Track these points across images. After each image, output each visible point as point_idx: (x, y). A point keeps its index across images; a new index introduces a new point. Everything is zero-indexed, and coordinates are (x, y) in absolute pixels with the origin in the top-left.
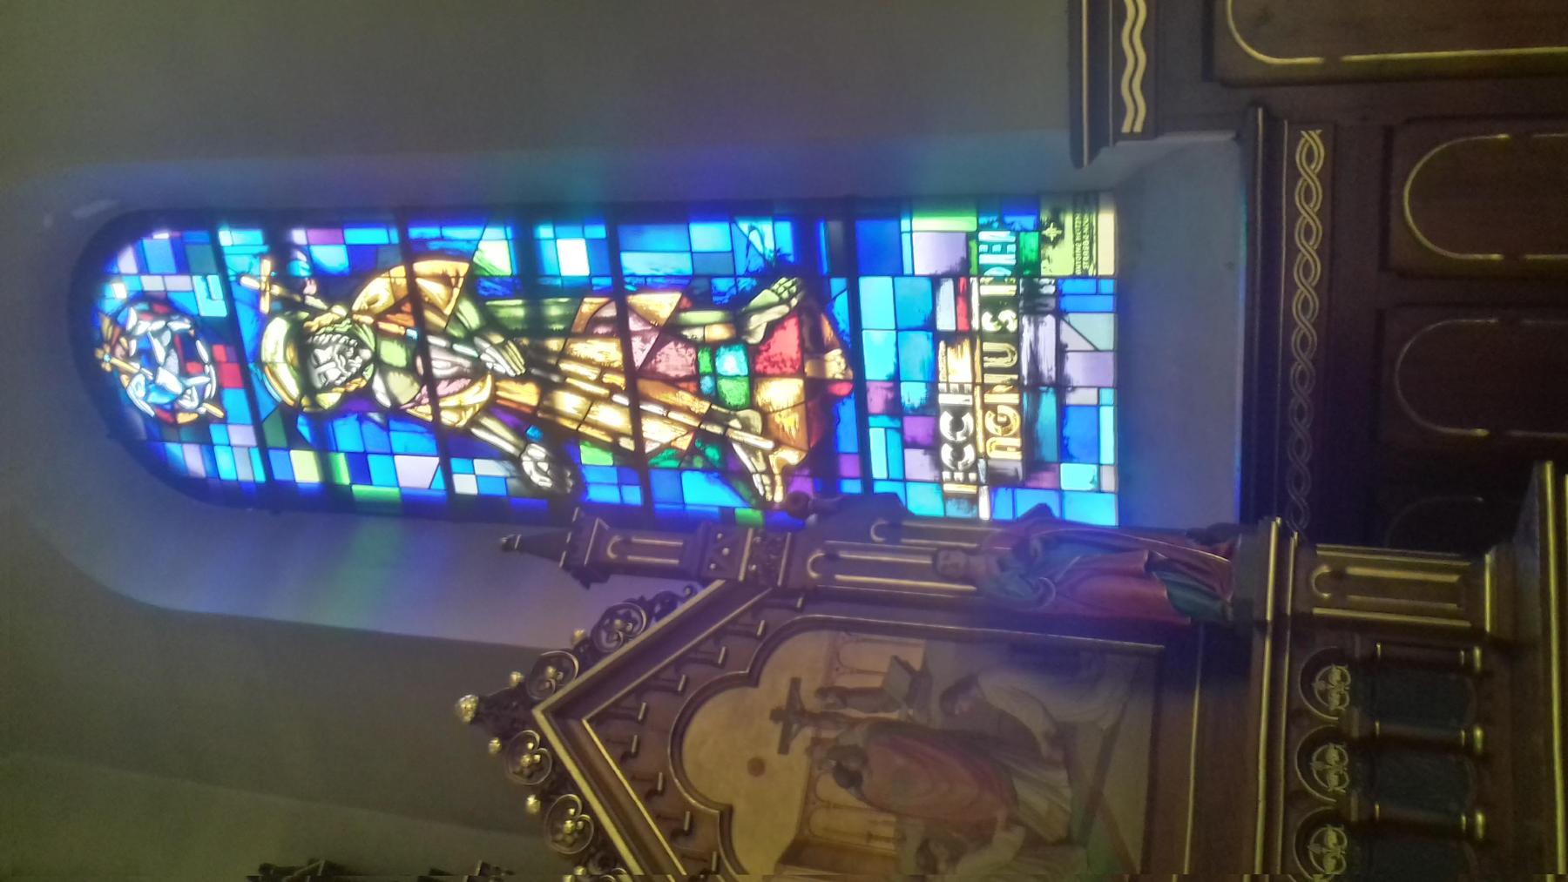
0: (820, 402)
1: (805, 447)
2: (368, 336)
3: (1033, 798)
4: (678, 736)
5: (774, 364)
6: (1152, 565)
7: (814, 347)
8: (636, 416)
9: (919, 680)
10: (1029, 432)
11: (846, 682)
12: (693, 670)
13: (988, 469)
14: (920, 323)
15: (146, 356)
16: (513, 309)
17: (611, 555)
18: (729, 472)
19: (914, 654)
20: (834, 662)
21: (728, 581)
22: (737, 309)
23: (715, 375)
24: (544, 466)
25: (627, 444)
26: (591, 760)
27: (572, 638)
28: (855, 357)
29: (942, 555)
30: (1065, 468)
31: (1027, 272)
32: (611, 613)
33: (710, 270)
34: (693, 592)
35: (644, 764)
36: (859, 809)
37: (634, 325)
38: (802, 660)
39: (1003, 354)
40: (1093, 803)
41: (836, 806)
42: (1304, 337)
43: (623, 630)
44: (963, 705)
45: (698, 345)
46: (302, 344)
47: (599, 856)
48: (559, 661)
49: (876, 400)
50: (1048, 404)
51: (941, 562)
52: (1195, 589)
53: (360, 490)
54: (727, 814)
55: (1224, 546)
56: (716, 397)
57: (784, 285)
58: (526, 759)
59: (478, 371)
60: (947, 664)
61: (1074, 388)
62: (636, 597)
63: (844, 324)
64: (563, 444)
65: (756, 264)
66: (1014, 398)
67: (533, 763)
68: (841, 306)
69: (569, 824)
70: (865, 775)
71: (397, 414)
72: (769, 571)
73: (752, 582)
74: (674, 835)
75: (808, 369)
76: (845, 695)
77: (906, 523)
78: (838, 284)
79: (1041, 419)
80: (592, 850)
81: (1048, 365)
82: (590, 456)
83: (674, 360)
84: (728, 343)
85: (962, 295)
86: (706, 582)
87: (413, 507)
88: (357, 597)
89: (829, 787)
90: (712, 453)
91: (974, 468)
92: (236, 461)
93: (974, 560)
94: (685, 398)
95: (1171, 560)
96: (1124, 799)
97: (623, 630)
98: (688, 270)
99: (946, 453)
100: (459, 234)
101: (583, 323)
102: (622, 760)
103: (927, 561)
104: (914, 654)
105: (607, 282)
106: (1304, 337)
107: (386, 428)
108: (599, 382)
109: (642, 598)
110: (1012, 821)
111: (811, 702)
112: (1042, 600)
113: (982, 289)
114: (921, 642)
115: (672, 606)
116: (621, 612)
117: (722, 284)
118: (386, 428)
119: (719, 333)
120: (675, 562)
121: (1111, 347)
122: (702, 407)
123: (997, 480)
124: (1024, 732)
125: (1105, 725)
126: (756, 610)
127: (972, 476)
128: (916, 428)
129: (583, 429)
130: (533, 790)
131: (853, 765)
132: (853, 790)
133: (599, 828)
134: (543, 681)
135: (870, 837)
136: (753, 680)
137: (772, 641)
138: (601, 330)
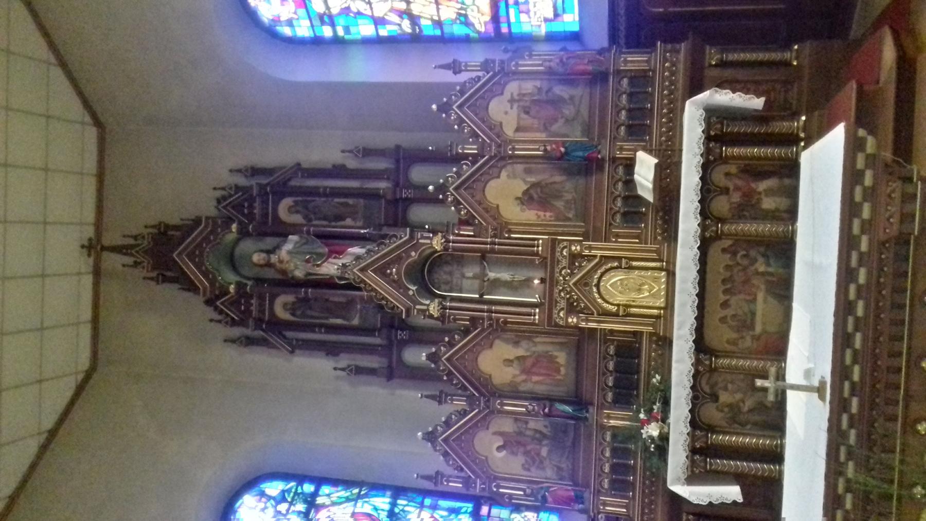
3: (566, 112)
4: (487, 108)
6: (589, 61)
8: (438, 9)
9: (540, 89)
11: (524, 92)
18: (468, 24)
20: (520, 86)
38: (513, 88)
40: (578, 112)
44: (550, 94)
53: (347, 37)
54: (501, 123)
64: (414, 20)
71: (359, 13)
72: (503, 69)
76: (524, 95)
82: (423, 22)
87: (367, 42)
88: (360, 70)
90: (462, 19)
92: (303, 30)
96: (585, 112)
99: (532, 14)
107: (355, 17)
111: (516, 98)
118: (355, 17)
122: (459, 6)
123: (546, 20)
136: (502, 94)
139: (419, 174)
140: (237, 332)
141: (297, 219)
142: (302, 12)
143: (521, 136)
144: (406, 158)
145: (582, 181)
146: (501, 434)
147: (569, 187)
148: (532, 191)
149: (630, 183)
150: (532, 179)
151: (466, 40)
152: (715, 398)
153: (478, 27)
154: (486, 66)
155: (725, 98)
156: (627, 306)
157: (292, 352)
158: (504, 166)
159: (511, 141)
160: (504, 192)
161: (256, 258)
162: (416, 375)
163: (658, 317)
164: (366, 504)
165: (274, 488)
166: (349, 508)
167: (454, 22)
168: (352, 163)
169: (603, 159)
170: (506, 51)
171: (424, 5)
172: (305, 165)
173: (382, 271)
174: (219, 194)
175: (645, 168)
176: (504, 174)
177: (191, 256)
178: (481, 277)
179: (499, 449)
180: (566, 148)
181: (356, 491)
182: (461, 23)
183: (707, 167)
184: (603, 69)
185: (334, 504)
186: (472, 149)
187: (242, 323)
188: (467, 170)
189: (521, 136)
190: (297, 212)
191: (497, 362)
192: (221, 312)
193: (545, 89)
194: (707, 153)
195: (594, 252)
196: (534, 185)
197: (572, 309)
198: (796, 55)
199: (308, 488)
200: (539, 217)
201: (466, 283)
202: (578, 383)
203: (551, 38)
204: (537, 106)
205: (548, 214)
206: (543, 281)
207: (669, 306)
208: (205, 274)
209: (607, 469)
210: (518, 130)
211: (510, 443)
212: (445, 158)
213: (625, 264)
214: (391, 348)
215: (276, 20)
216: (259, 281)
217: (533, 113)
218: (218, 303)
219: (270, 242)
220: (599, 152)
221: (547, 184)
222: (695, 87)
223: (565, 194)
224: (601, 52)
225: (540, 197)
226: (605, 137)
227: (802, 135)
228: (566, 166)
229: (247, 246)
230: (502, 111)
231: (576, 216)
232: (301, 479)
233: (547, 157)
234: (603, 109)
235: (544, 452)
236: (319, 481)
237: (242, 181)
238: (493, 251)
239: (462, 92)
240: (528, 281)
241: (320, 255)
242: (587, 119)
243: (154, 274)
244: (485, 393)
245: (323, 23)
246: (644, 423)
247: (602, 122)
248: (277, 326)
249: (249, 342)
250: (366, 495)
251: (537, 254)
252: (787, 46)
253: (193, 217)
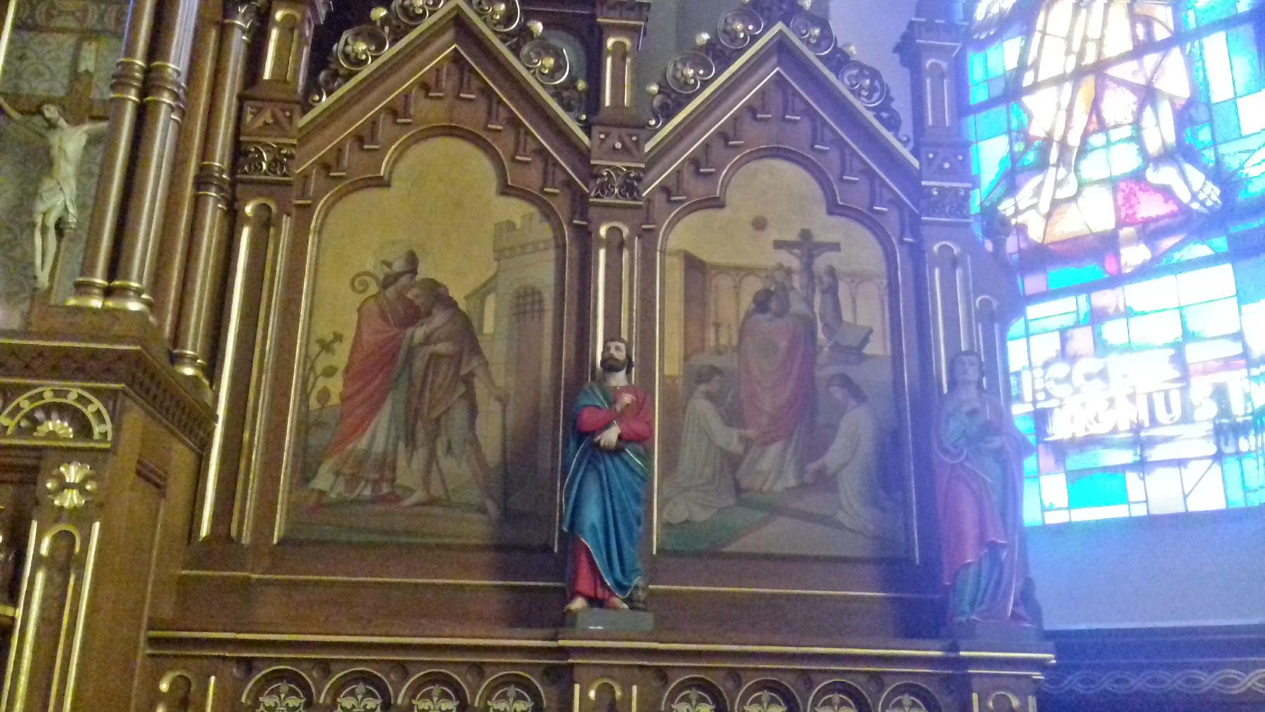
0: (1102, 247)
1: (1049, 239)
5: (1127, 199)
7: (1150, 232)
8: (1059, 81)
9: (856, 353)
12: (834, 156)
13: (1051, 410)
14: (1191, 327)
17: (928, 63)
18: (1011, 180)
19: (877, 347)
20: (859, 278)
21: (920, 172)
22: (1181, 153)
23: (1109, 144)
24: (995, 10)
25: (1028, 80)
26: (747, 78)
27: (848, 45)
28: (1143, 272)
29: (974, 358)
30: (1061, 478)
32: (875, 75)
33: (1218, 120)
34: (905, 143)
35: (751, 129)
36: (738, 316)
37: (1151, 59)
39: (1169, 410)
40: (774, 509)
41: (738, 294)
42: (1235, 681)
43: (861, 88)
44: (838, 393)
45: (1137, 124)
47: (669, 101)
48: (827, 35)
49: (1104, 299)
50: (1128, 456)
51: (965, 358)
52: (978, 590)
54: (716, 203)
55: (1021, 611)
57: (1212, 193)
58: (739, 26)
60: (874, 376)
61: (1143, 479)
62: (893, 94)
63: (1177, 256)
65: (1232, 163)
66: (1124, 426)
67: (736, 32)
68: (1199, 250)
69: (691, 72)
70: (768, 316)
72: (935, 207)
73: (924, 193)
74: (695, 162)
75: (1127, 231)
76: (832, 291)
77: (996, 326)
78: (1221, 243)
79: (1106, 451)
80: (673, 96)
81: (1155, 454)
83: (1118, 106)
84: (1143, 151)
85: (1227, 364)
86: (915, 152)
89: (753, 286)
90: (1031, 157)
91: (1049, 396)
93: (973, 388)
95: (1001, 565)
96: (776, 535)
97: (861, 88)
98: (1215, 99)
101: (1145, 12)
102: (751, 109)
103: (964, 347)
104: (877, 347)
105: (1191, 24)
106: (1235, 681)
108: (1085, 40)
109: (892, 99)
110: (747, 442)
112: (946, 452)
113: (1236, 381)
114: (889, 352)
115: (889, 128)
116: (877, 83)
117: (1204, 135)
119: (1153, 147)
120: (930, 122)
121: (1191, 509)
122: (1074, 140)
123: (1041, 417)
124: (825, 448)
125: (841, 516)
126: (896, 202)
127: (1041, 396)
128: (1082, 340)
129: (1037, 36)
130: (715, 36)
131: (774, 305)
132: (753, 306)
133: (691, 98)
134: (806, 26)
135: (717, 325)
136: (834, 208)
137: (869, 220)
138: (1141, 31)
143: (671, 280)
145: (476, 529)
147: (452, 476)
148: (439, 318)
150: (490, 323)
158: (548, 213)
159: (647, 236)
169: (563, 621)
171: (1069, 39)
176: (517, 210)
180: (617, 451)
182: (1014, 158)
184: (965, 610)
189: (671, 282)
193: (858, 374)
196: (466, 330)
200: (326, 347)
205: (336, 386)
210: (693, 265)
217: (764, 322)
220: (594, 601)
221: (468, 381)
223: (421, 454)
225: (411, 353)
226: (663, 628)
228: (545, 464)
230: (765, 211)
231: (322, 503)
233: (580, 374)
234: (770, 616)
242: (747, 543)
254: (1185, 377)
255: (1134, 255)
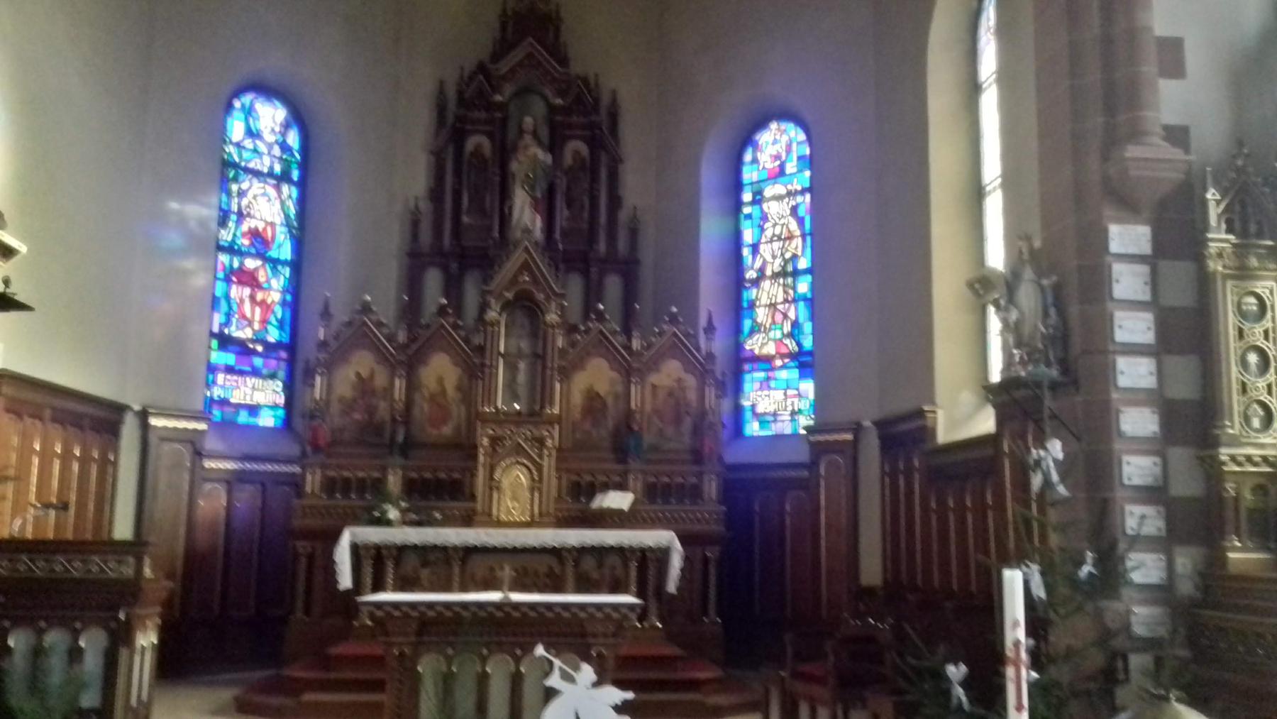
0: (768, 359)
2: (782, 221)
7: (782, 356)
10: (765, 414)
15: (775, 142)
16: (790, 268)
22: (791, 335)
31: (800, 411)
38: (691, 381)
46: (779, 198)
49: (770, 374)
56: (770, 329)
57: (796, 349)
59: (774, 257)
64: (756, 282)
71: (762, 230)
83: (779, 317)
85: (795, 396)
88: (711, 229)
92: (749, 174)
94: (770, 320)
96: (672, 445)
100: (808, 251)
113: (796, 400)
123: (753, 406)
139: (613, 285)
140: (451, 93)
141: (568, 160)
142: (765, 175)
144: (629, 269)
146: (372, 376)
149: (606, 487)
150: (610, 401)
151: (738, 329)
152: (425, 564)
153: (750, 342)
154: (710, 356)
155: (676, 562)
156: (498, 489)
157: (432, 152)
160: (597, 375)
161: (528, 121)
162: (413, 284)
163: (490, 515)
164: (283, 237)
165: (293, 139)
166: (278, 219)
167: (754, 321)
168: (623, 215)
170: (723, 374)
172: (621, 167)
173: (525, 267)
174: (592, 82)
175: (618, 500)
177: (530, 56)
178: (520, 355)
179: (358, 375)
181: (295, 224)
183: (620, 551)
185: (282, 203)
186: (636, 344)
187: (461, 101)
188: (618, 341)
190: (574, 159)
191: (441, 370)
192: (471, 78)
194: (632, 550)
195: (546, 458)
196: (604, 404)
197: (495, 441)
198: (713, 619)
199: (295, 175)
201: (513, 342)
202: (424, 445)
203: (738, 411)
204: (676, 407)
206: (519, 413)
207: (500, 524)
208: (512, 71)
209: (346, 474)
210: (654, 387)
211: (364, 386)
212: (628, 322)
213: (536, 485)
214: (438, 256)
215: (756, 147)
216: (504, 121)
218: (481, 77)
219: (544, 133)
222: (684, 539)
224: (720, 459)
227: (646, 624)
229: (539, 108)
230: (670, 372)
232: (304, 166)
233: (629, 414)
234: (670, 462)
235: (357, 416)
236: (302, 185)
237: (605, 100)
238: (544, 367)
239: (687, 335)
240: (516, 398)
241: (532, 188)
243: (510, 13)
244: (409, 361)
245: (755, 194)
246: (397, 506)
247: (660, 462)
248: (458, 136)
249: (441, 109)
250: (292, 236)
251: (542, 407)
252: (720, 614)
253: (563, 14)
254: (785, 399)
255: (778, 363)
